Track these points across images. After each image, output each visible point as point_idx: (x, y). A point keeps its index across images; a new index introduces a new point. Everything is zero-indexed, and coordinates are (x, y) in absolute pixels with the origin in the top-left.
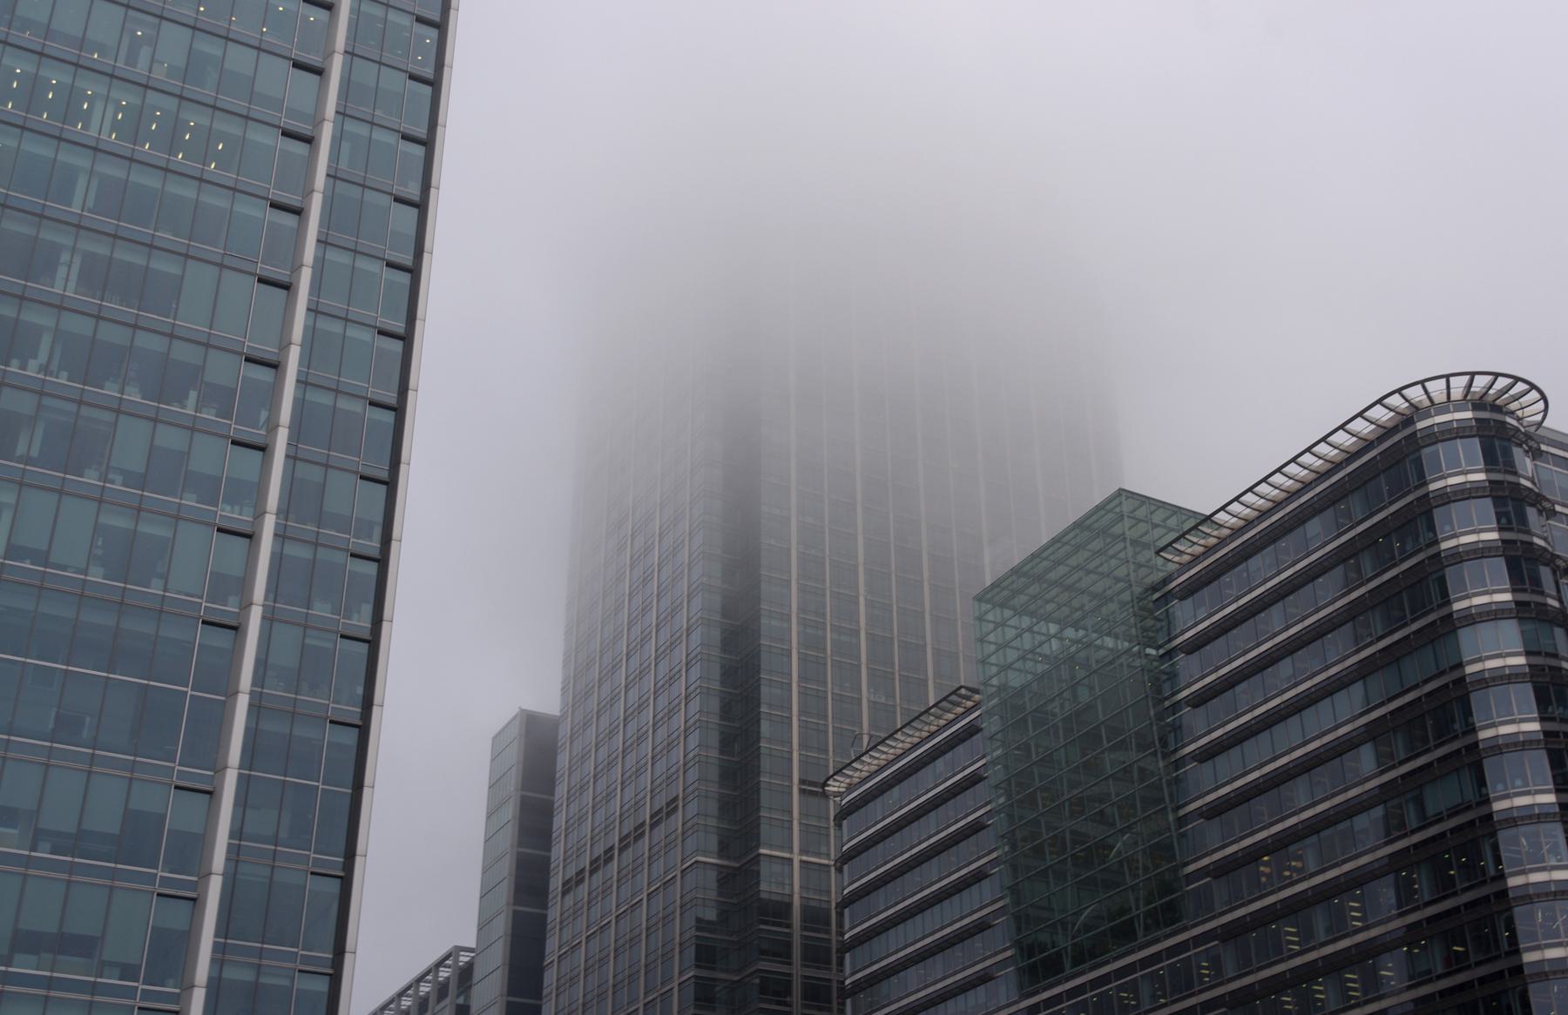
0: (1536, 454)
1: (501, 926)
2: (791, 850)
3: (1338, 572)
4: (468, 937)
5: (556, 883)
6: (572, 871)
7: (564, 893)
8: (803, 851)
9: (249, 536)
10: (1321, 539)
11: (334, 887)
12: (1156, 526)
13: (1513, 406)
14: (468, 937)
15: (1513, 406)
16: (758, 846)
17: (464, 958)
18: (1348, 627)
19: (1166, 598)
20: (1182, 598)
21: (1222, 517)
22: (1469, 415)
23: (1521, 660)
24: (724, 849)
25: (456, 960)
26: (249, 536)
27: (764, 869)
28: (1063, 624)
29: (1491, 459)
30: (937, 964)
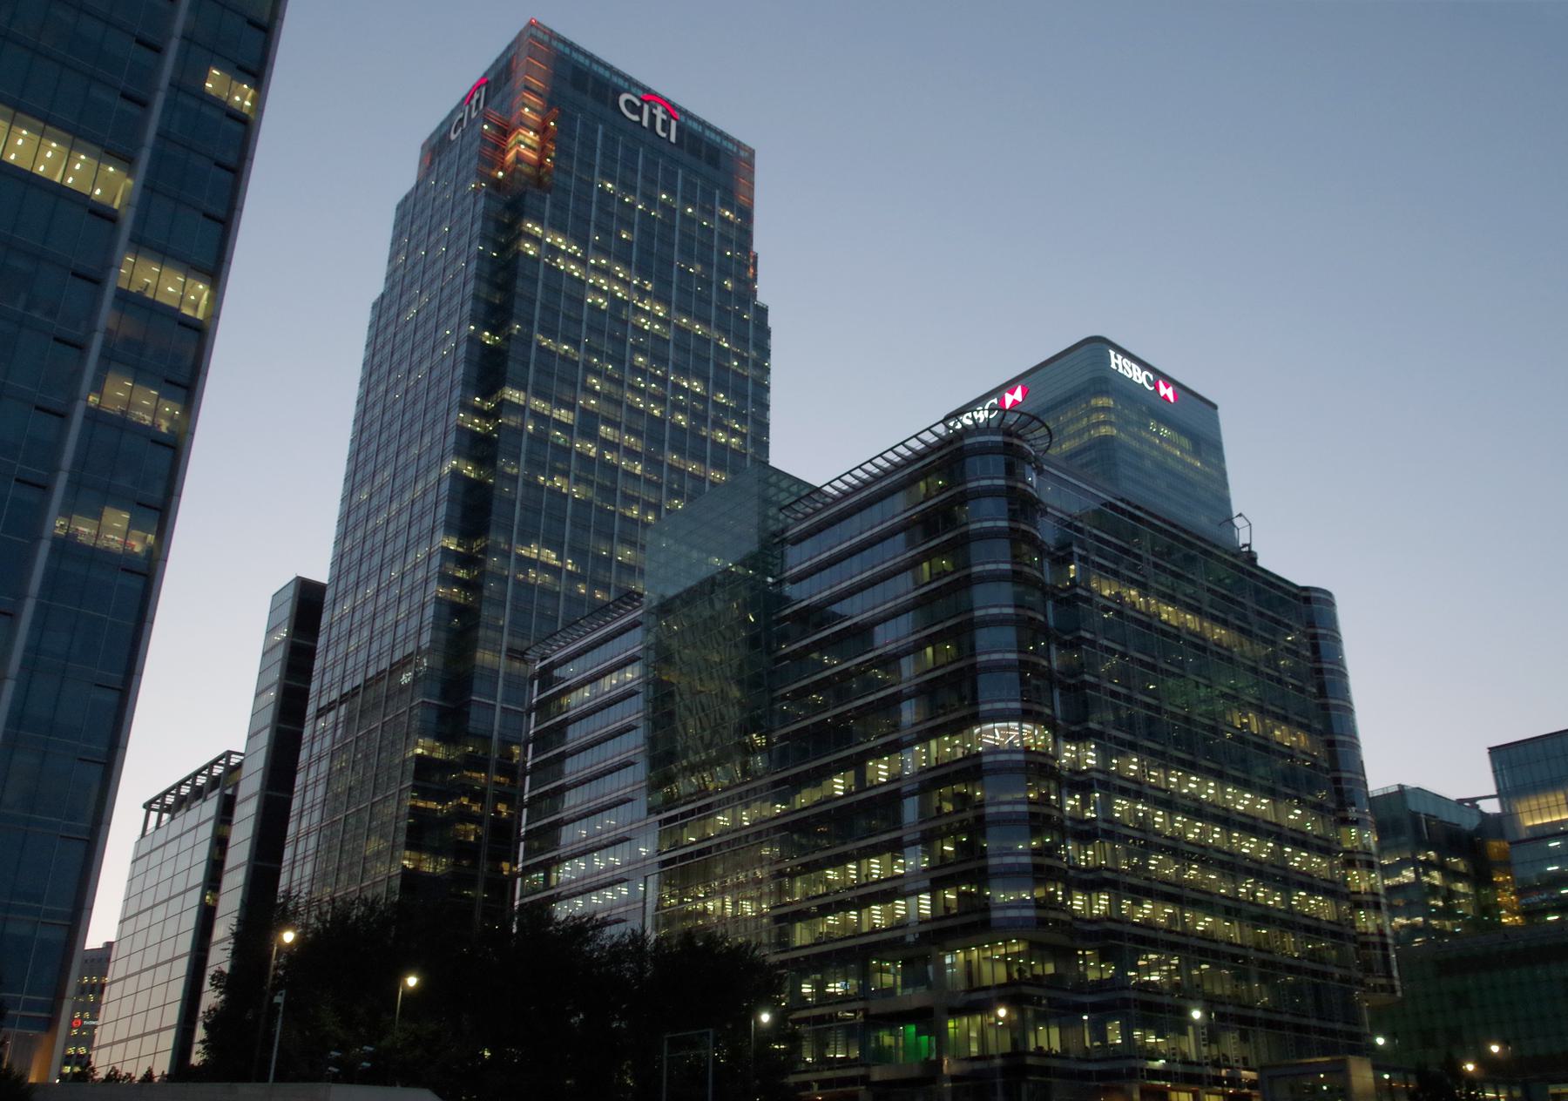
0: (1040, 471)
1: (264, 739)
2: (495, 698)
3: (901, 537)
4: (237, 741)
5: (311, 710)
6: (323, 703)
7: (318, 717)
8: (505, 700)
9: (61, 416)
10: (898, 509)
11: (111, 698)
12: (783, 490)
13: (1030, 436)
14: (237, 741)
15: (1030, 436)
16: (471, 693)
17: (234, 760)
18: (909, 573)
19: (784, 541)
20: (794, 544)
21: (828, 489)
22: (999, 438)
23: (1010, 611)
24: (444, 694)
25: (228, 761)
26: (61, 416)
27: (474, 712)
28: (935, 887)
29: (1010, 471)
30: (854, 563)
